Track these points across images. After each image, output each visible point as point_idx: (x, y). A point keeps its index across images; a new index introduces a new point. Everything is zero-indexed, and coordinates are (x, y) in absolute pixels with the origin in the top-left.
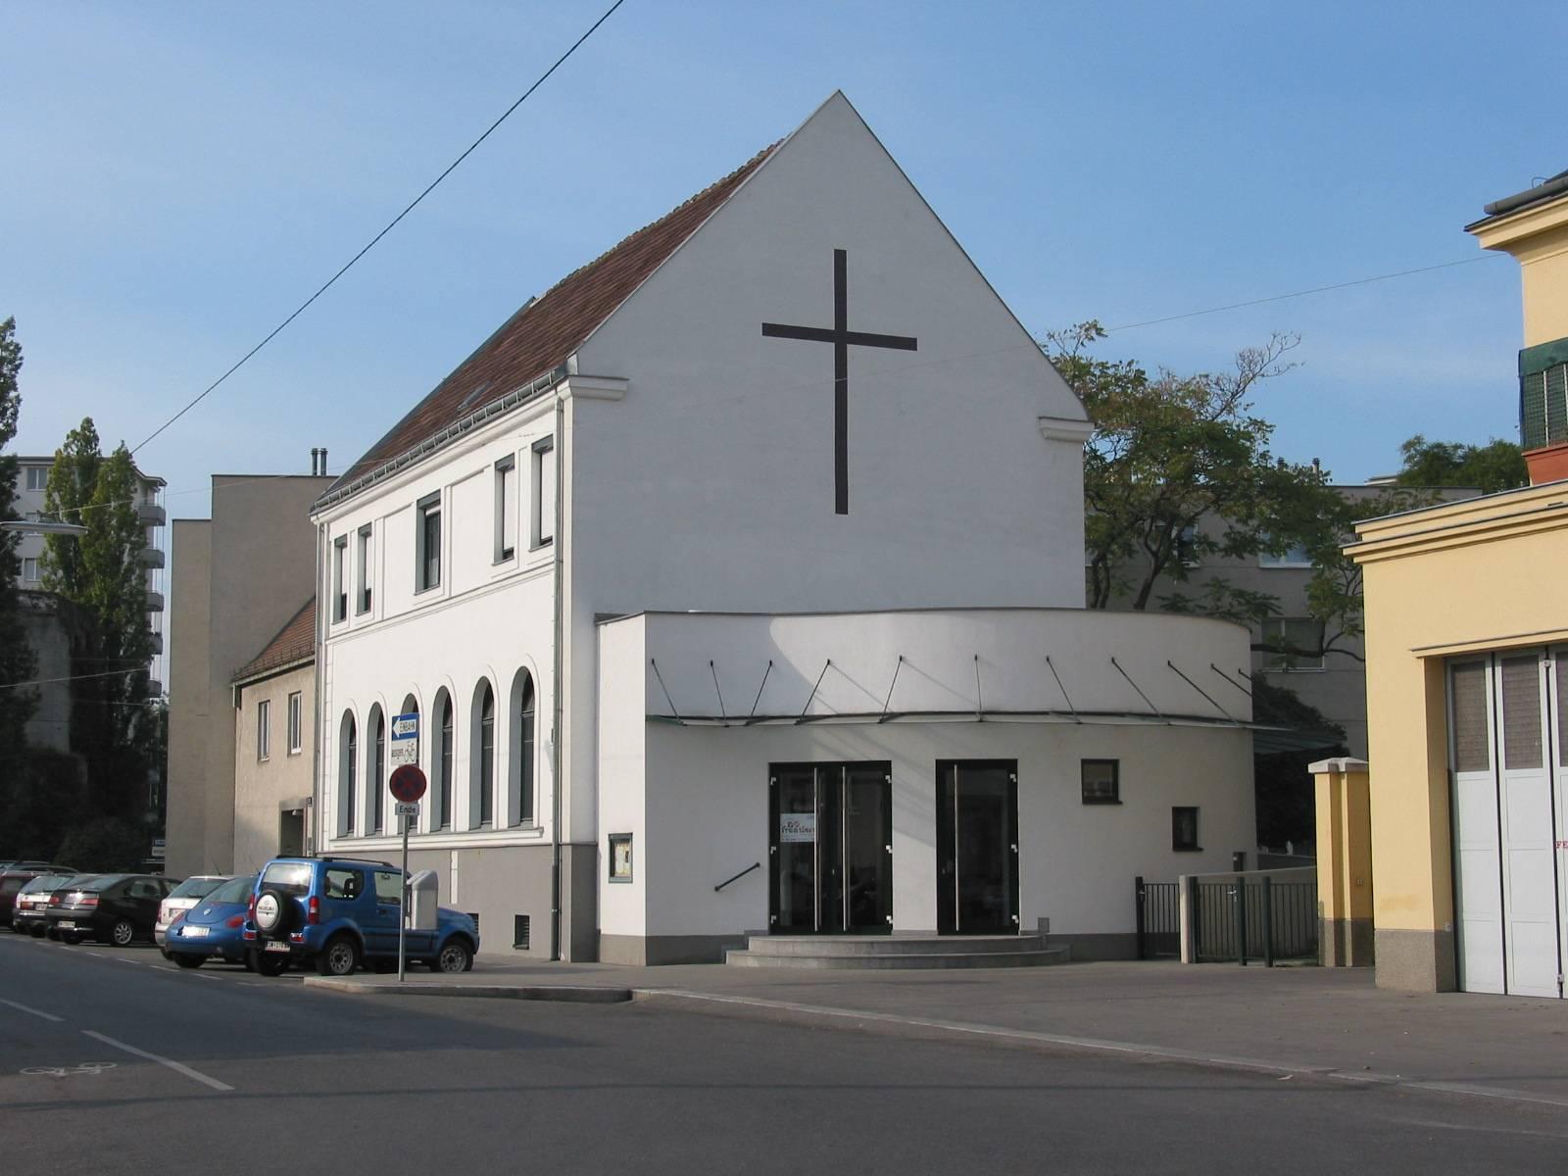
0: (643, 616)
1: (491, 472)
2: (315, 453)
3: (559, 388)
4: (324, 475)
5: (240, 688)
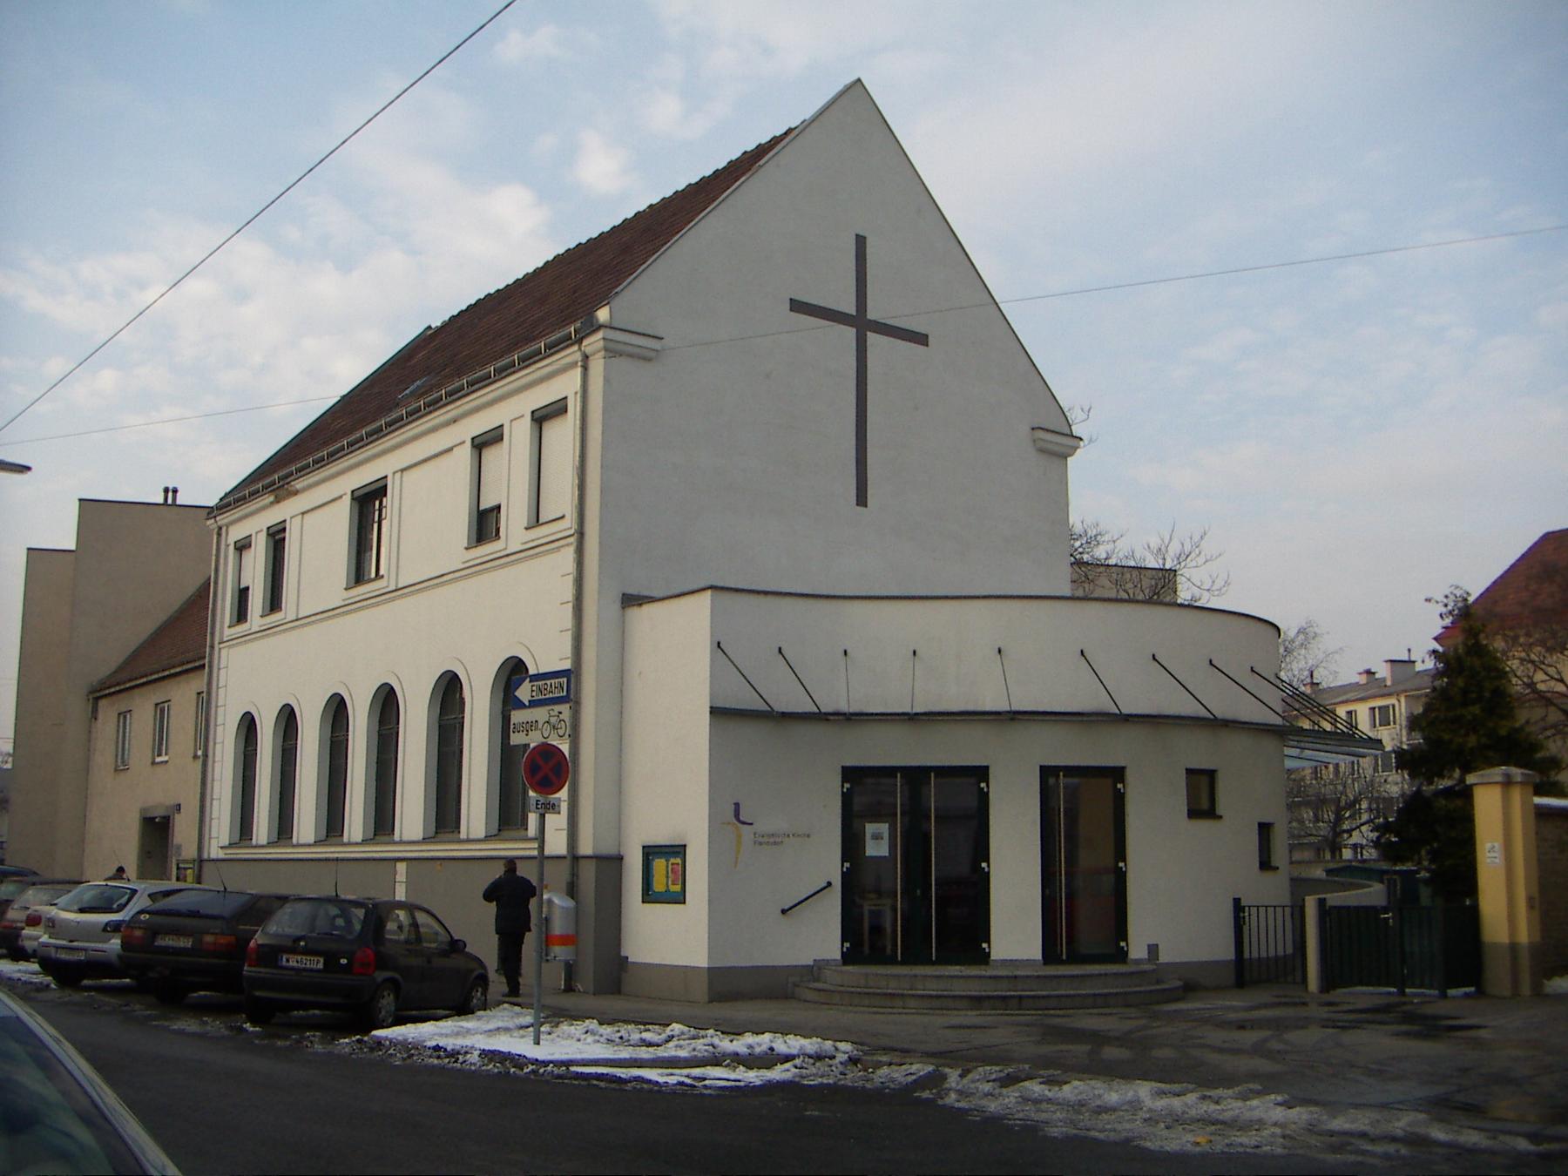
0: (709, 593)
1: (466, 452)
2: (166, 490)
3: (585, 342)
4: (174, 504)
5: (97, 699)
